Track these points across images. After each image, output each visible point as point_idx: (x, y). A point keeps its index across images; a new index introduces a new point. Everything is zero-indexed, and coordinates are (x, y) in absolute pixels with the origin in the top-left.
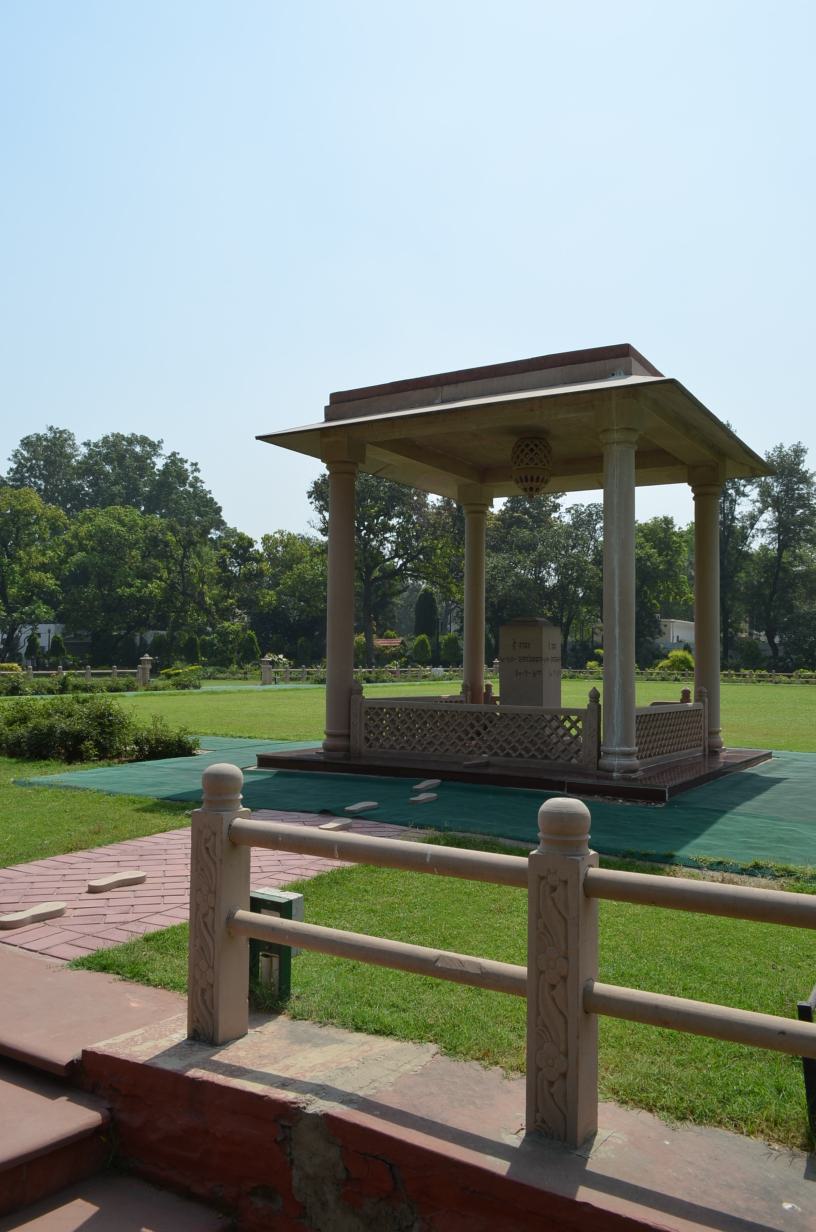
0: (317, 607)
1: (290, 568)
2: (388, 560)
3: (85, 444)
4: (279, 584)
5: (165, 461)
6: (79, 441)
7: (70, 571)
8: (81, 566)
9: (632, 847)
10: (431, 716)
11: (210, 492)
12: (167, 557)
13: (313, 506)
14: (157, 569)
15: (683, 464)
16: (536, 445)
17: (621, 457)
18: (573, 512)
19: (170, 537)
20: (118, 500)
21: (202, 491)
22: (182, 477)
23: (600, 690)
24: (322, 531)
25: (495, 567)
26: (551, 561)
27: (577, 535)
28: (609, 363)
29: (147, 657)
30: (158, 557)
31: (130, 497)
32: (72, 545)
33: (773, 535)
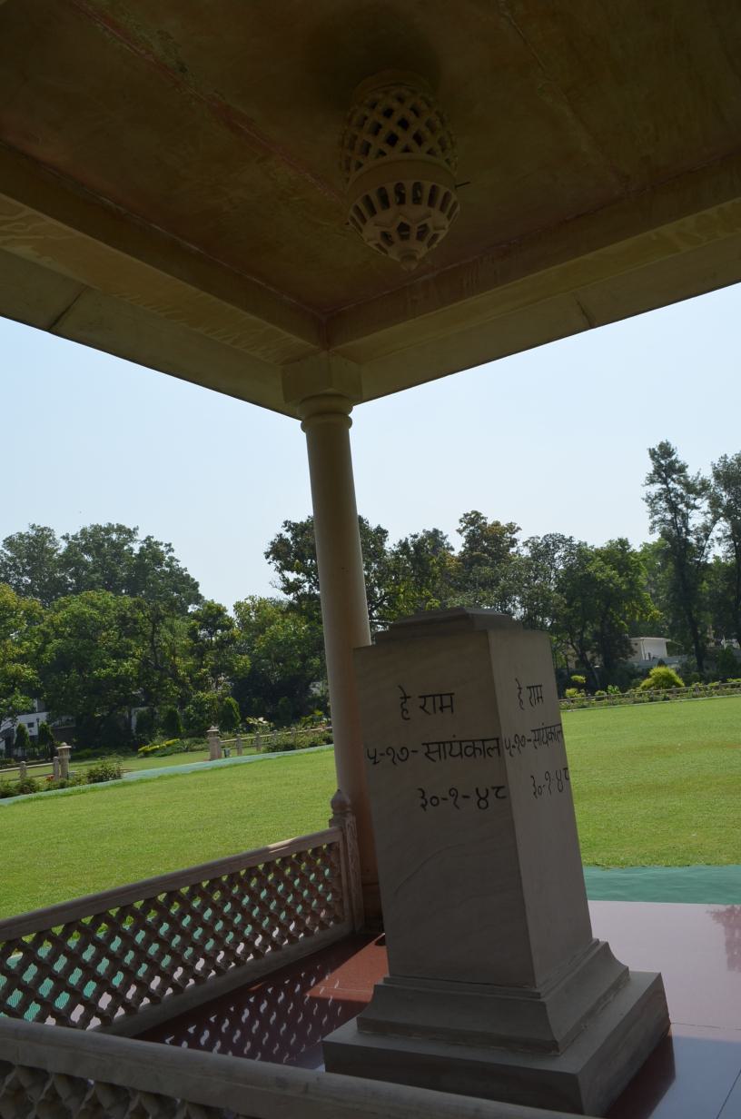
0: (293, 666)
1: (263, 631)
3: (64, 538)
5: (141, 545)
6: (58, 536)
7: (51, 659)
8: (58, 651)
11: (186, 569)
13: (273, 566)
14: (129, 647)
18: (530, 545)
24: (283, 589)
26: (515, 594)
29: (65, 746)
31: (111, 584)
32: (48, 634)
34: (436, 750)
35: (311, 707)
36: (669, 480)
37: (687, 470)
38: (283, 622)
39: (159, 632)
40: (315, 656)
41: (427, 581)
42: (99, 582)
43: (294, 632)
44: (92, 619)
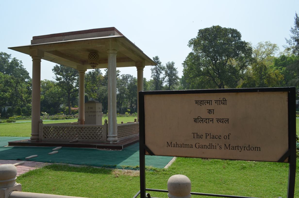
0: (56, 100)
1: (48, 89)
4: (45, 94)
5: (12, 60)
9: (105, 164)
10: (62, 128)
11: (25, 69)
13: (54, 73)
14: (8, 89)
15: (134, 61)
16: (94, 54)
17: (112, 58)
18: (122, 76)
19: (12, 81)
22: (17, 64)
23: (107, 119)
25: (103, 89)
27: (123, 82)
28: (109, 32)
30: (9, 86)
33: (168, 82)
35: (60, 111)
38: (54, 87)
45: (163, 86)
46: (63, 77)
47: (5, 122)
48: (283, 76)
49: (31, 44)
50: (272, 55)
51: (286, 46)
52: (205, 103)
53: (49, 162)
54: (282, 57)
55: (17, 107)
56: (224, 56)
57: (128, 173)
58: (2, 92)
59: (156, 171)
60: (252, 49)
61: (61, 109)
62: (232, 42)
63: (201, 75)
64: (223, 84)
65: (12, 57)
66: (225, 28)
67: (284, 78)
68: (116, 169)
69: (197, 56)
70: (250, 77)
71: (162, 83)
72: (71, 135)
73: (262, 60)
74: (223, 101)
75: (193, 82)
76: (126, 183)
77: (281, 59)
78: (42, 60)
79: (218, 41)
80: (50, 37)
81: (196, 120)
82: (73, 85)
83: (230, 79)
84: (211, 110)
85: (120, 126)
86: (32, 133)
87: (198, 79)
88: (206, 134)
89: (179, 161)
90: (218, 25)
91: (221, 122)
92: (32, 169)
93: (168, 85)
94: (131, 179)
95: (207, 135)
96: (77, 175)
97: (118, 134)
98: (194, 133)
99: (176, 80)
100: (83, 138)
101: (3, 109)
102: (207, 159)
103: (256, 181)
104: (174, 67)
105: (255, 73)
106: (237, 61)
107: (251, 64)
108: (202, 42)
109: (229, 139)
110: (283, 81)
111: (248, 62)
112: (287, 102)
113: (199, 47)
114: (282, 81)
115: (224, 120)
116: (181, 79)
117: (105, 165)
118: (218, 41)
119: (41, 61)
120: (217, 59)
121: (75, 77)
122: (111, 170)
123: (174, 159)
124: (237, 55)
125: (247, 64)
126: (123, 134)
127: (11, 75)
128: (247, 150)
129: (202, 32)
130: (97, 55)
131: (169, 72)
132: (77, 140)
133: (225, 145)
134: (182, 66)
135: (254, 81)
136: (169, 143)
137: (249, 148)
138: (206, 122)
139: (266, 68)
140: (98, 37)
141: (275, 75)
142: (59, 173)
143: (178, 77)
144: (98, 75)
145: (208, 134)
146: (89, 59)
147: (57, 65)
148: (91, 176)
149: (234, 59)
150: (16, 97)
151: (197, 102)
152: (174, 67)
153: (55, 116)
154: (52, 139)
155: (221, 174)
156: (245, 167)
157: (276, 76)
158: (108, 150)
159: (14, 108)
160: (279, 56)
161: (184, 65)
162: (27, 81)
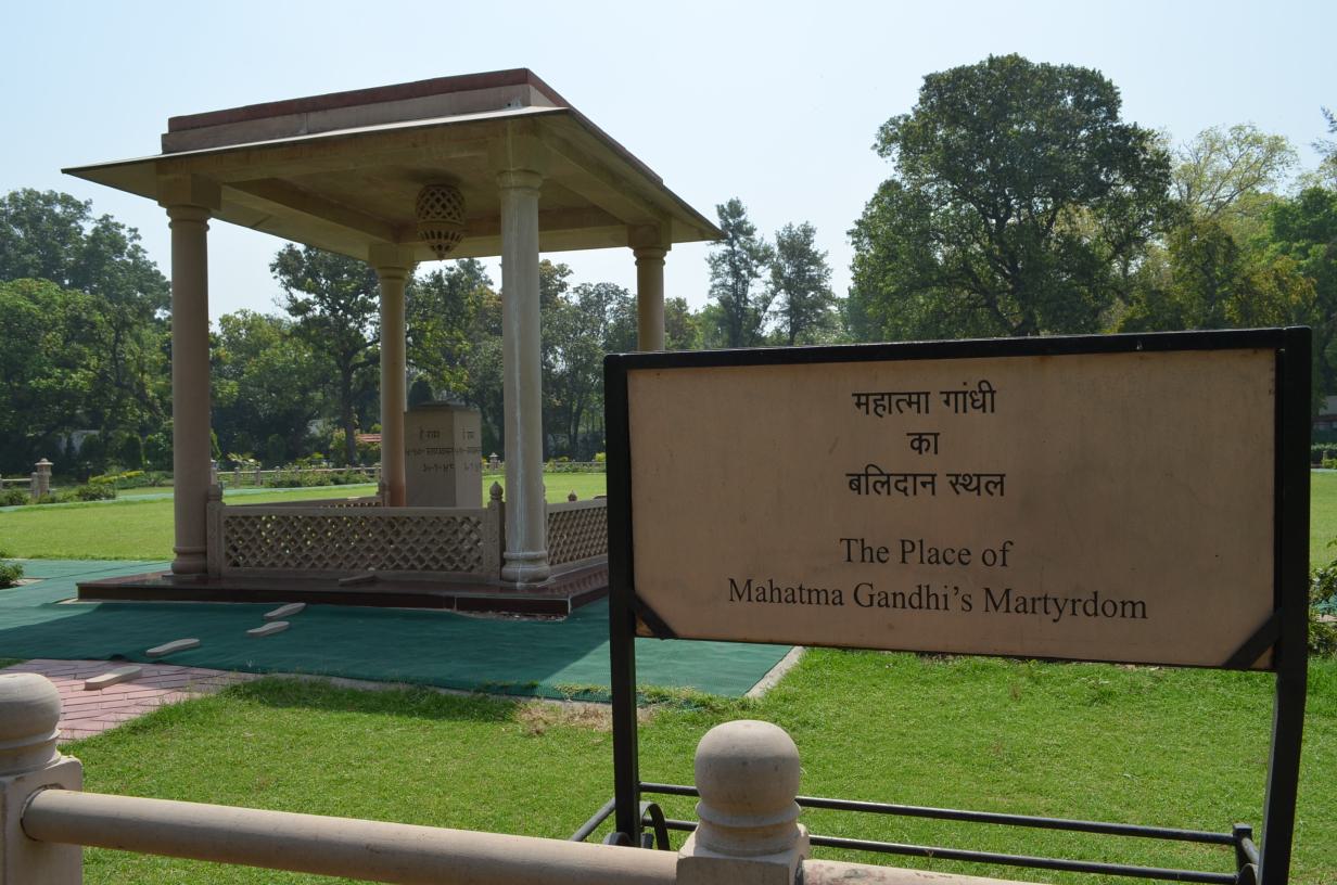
0: (290, 399)
1: (256, 354)
2: (370, 344)
5: (95, 225)
11: (155, 264)
12: (95, 341)
13: (278, 281)
14: (81, 356)
16: (443, 194)
17: (521, 212)
18: (581, 292)
19: (98, 317)
20: (31, 271)
21: (145, 263)
22: (117, 245)
23: (502, 483)
25: (496, 352)
26: (558, 345)
27: (585, 317)
28: (505, 91)
29: (45, 462)
30: (85, 340)
33: (786, 318)
34: (432, 451)
35: (307, 448)
36: (735, 242)
37: (755, 233)
38: (282, 345)
39: (123, 342)
40: (317, 389)
41: (460, 321)
42: (33, 265)
43: (295, 359)
44: (30, 315)
45: (764, 335)
46: (317, 300)
47: (70, 498)
48: (1313, 283)
49: (163, 153)
50: (1263, 190)
51: (1327, 146)
52: (900, 403)
53: (244, 669)
54: (1310, 197)
55: (123, 432)
56: (1039, 196)
57: (585, 716)
58: (58, 367)
59: (712, 708)
60: (1169, 159)
61: (313, 440)
62: (1076, 129)
63: (935, 283)
64: (1035, 324)
65: (96, 213)
66: (1046, 68)
67: (1315, 294)
68: (536, 700)
69: (918, 196)
70: (1160, 292)
71: (759, 320)
72: (347, 553)
73: (1216, 212)
74: (980, 396)
75: (895, 314)
76: (578, 758)
77: (1305, 207)
78: (212, 222)
79: (1016, 127)
80: (247, 120)
81: (859, 480)
82: (365, 336)
83: (1064, 299)
84: (924, 437)
85: (562, 510)
86: (177, 545)
87: (922, 301)
88: (903, 542)
89: (817, 664)
90: (1012, 53)
91: (969, 487)
92: (173, 698)
93: (786, 330)
94: (599, 744)
95: (908, 547)
96: (365, 725)
97: (552, 546)
98: (849, 541)
99: (822, 309)
100: (398, 567)
101: (65, 440)
102: (944, 654)
103: (1153, 756)
104: (811, 248)
105: (1180, 271)
106: (1100, 217)
107: (1166, 230)
108: (941, 133)
109: (1004, 564)
110: (1314, 306)
111: (1150, 223)
112: (1272, 397)
113: (924, 156)
114: (1308, 306)
115: (984, 480)
116: (843, 301)
117: (490, 683)
118: (1012, 126)
119: (208, 228)
120: (1009, 209)
121: (370, 300)
122: (513, 706)
123: (795, 655)
124: (1103, 188)
125: (1146, 230)
126: (575, 550)
127: (93, 292)
128: (1089, 615)
129: (939, 88)
130: (453, 195)
131: (788, 271)
132: (370, 575)
133: (988, 590)
134: (847, 242)
135: (1177, 310)
136: (741, 586)
137: (1096, 606)
138: (905, 490)
139: (1236, 248)
140: (454, 114)
141: (1276, 278)
142: (288, 716)
143: (829, 292)
144: (471, 286)
145: (913, 544)
146: (419, 215)
147: (291, 245)
148: (425, 730)
149: (1085, 209)
150: (116, 389)
151: (861, 400)
152: (813, 248)
153: (288, 472)
154: (262, 569)
155: (999, 722)
156: (1110, 694)
157: (1279, 284)
158: (506, 619)
159: (111, 439)
160: (1296, 192)
161: (856, 239)
162: (163, 318)
